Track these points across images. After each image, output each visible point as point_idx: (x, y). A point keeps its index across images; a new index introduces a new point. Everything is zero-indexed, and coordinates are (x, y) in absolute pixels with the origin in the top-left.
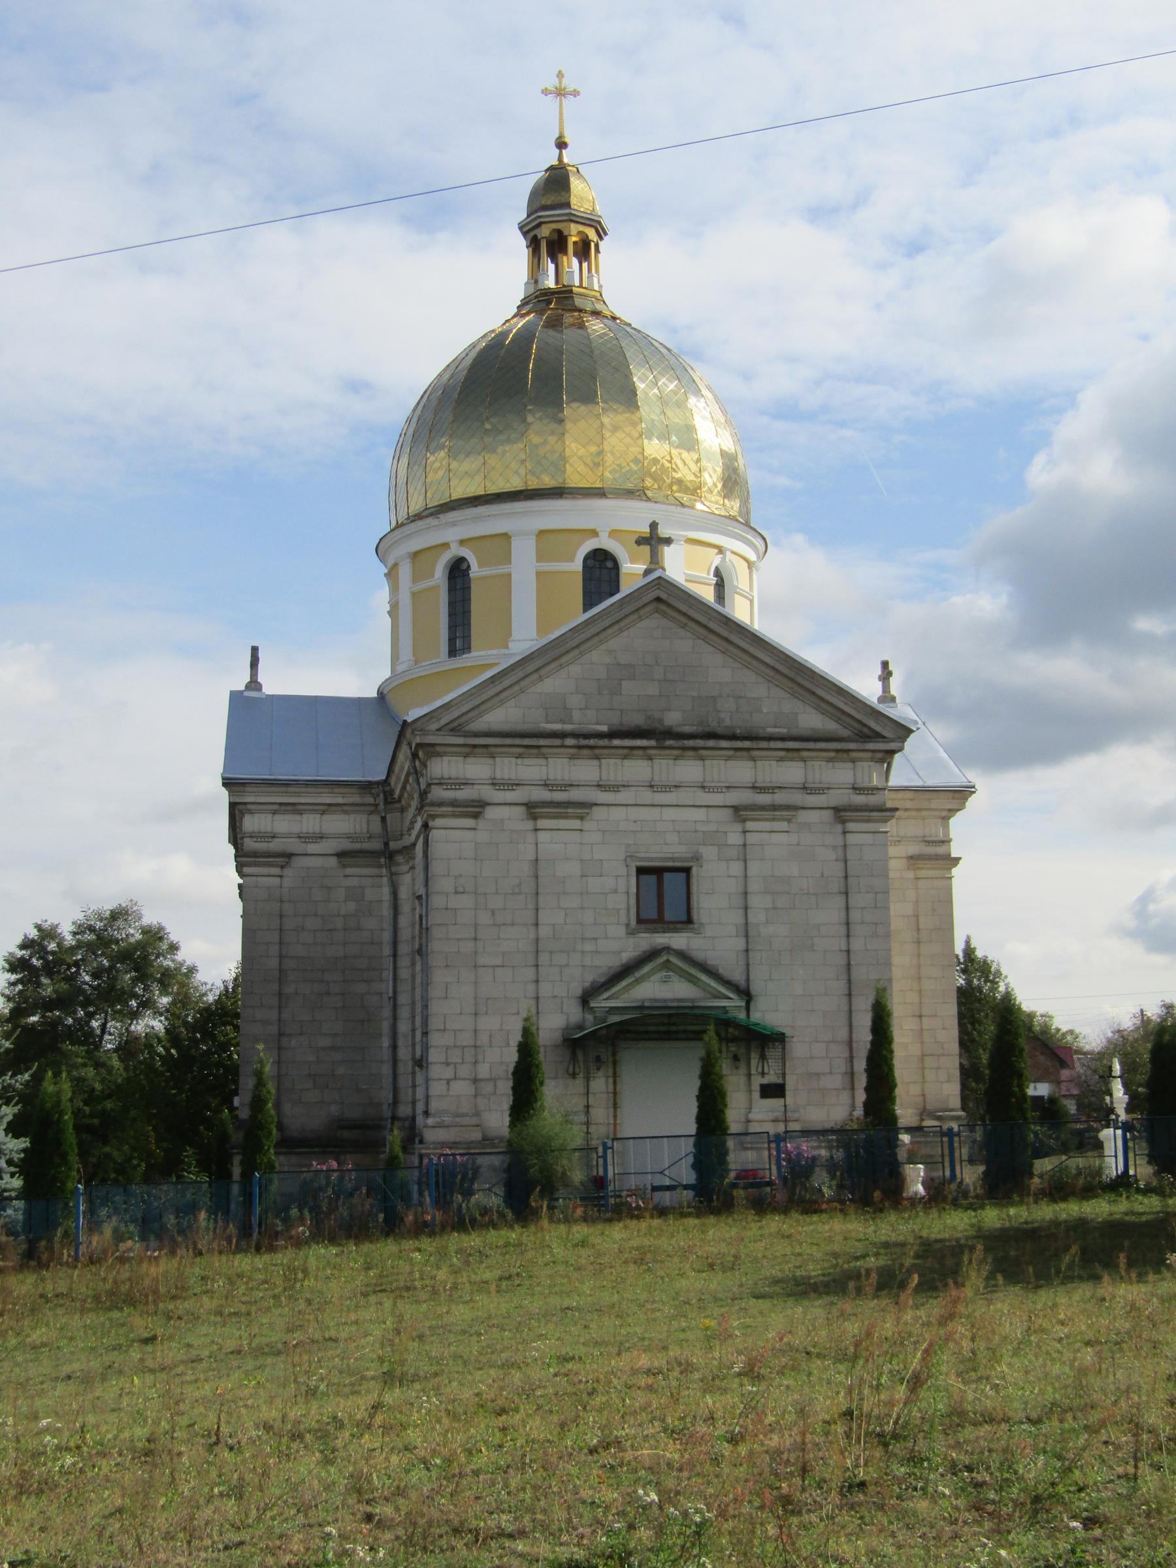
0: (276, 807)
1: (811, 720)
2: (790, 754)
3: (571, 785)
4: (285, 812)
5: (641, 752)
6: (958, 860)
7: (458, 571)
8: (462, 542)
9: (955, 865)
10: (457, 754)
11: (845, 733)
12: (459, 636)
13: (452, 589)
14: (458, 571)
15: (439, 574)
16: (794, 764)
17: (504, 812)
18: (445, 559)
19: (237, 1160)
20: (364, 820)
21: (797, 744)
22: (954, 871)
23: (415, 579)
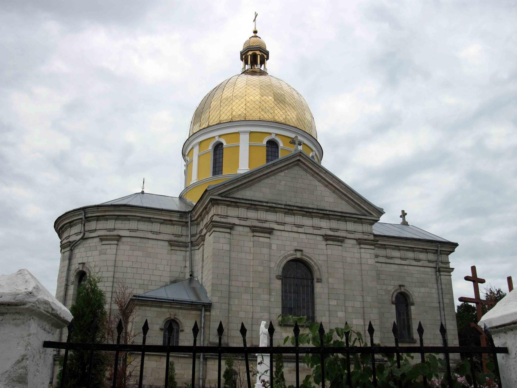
0: (162, 221)
1: (344, 207)
2: (358, 220)
3: (285, 223)
4: (145, 221)
5: (102, 218)
6: (453, 269)
7: (218, 147)
8: (220, 136)
9: (453, 271)
10: (244, 207)
11: (359, 213)
12: (217, 168)
13: (215, 154)
14: (218, 147)
15: (210, 147)
16: (342, 222)
17: (241, 229)
18: (213, 142)
19: (470, 304)
20: (180, 229)
21: (343, 217)
22: (452, 273)
23: (200, 151)
